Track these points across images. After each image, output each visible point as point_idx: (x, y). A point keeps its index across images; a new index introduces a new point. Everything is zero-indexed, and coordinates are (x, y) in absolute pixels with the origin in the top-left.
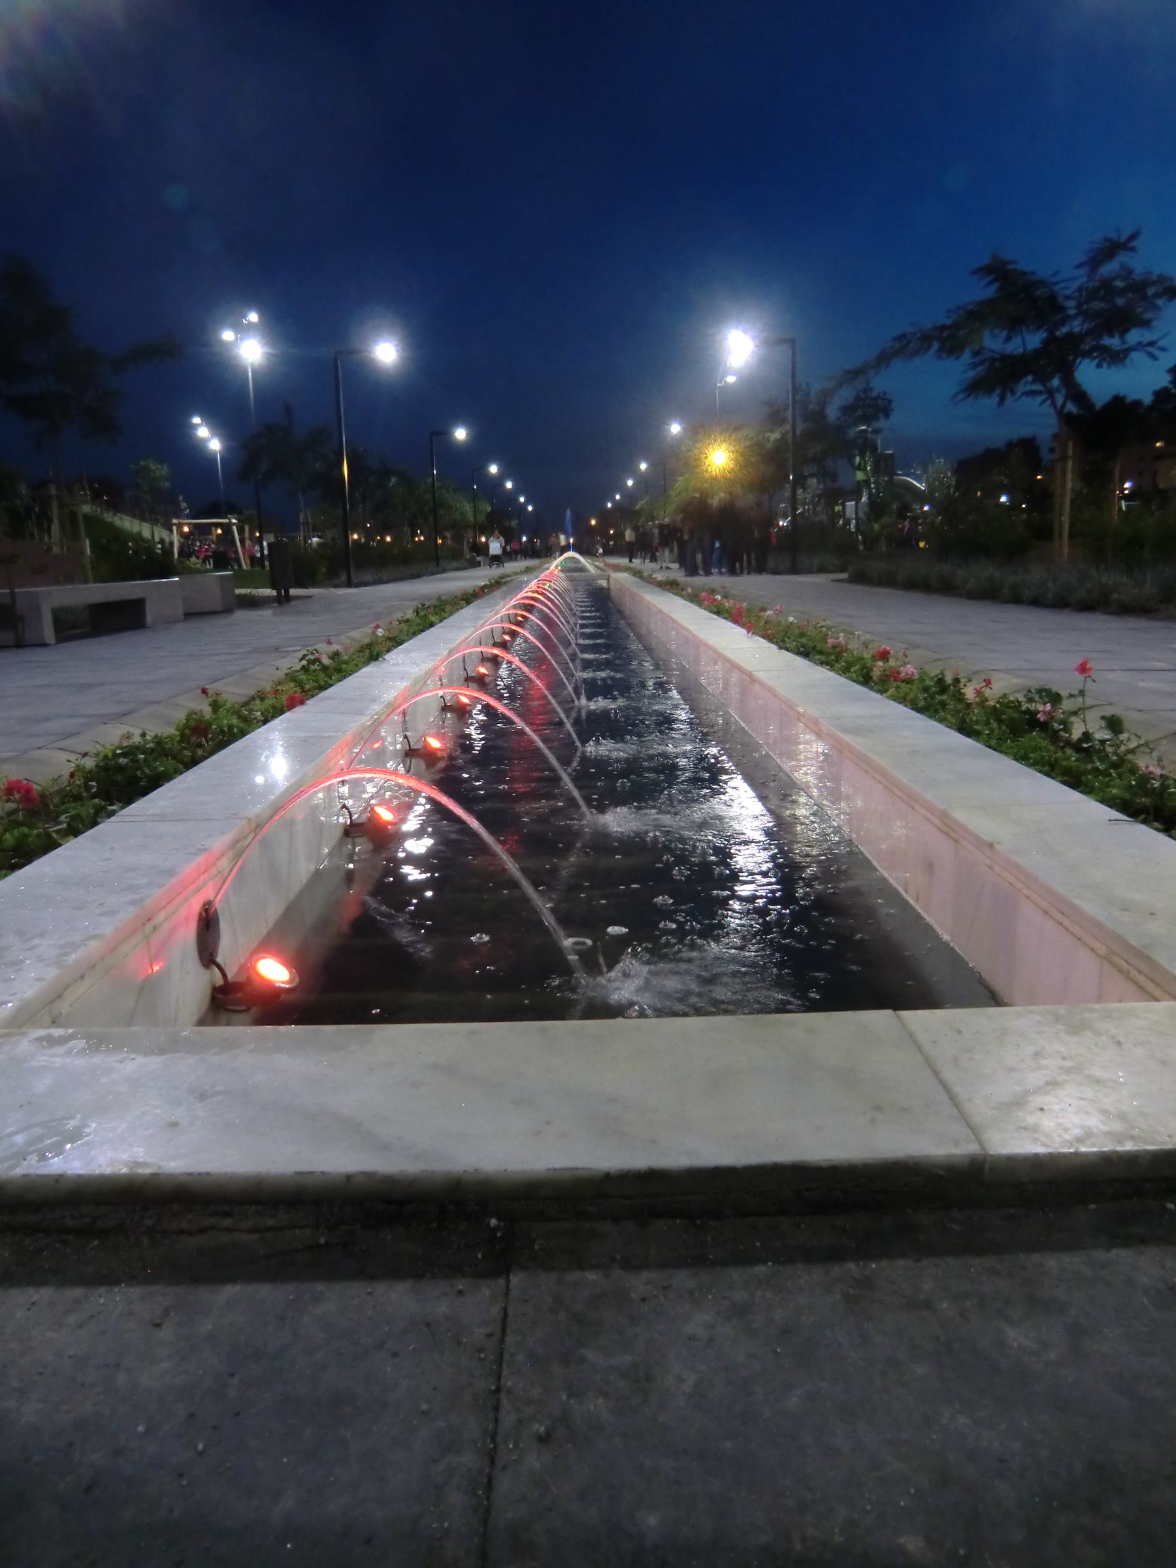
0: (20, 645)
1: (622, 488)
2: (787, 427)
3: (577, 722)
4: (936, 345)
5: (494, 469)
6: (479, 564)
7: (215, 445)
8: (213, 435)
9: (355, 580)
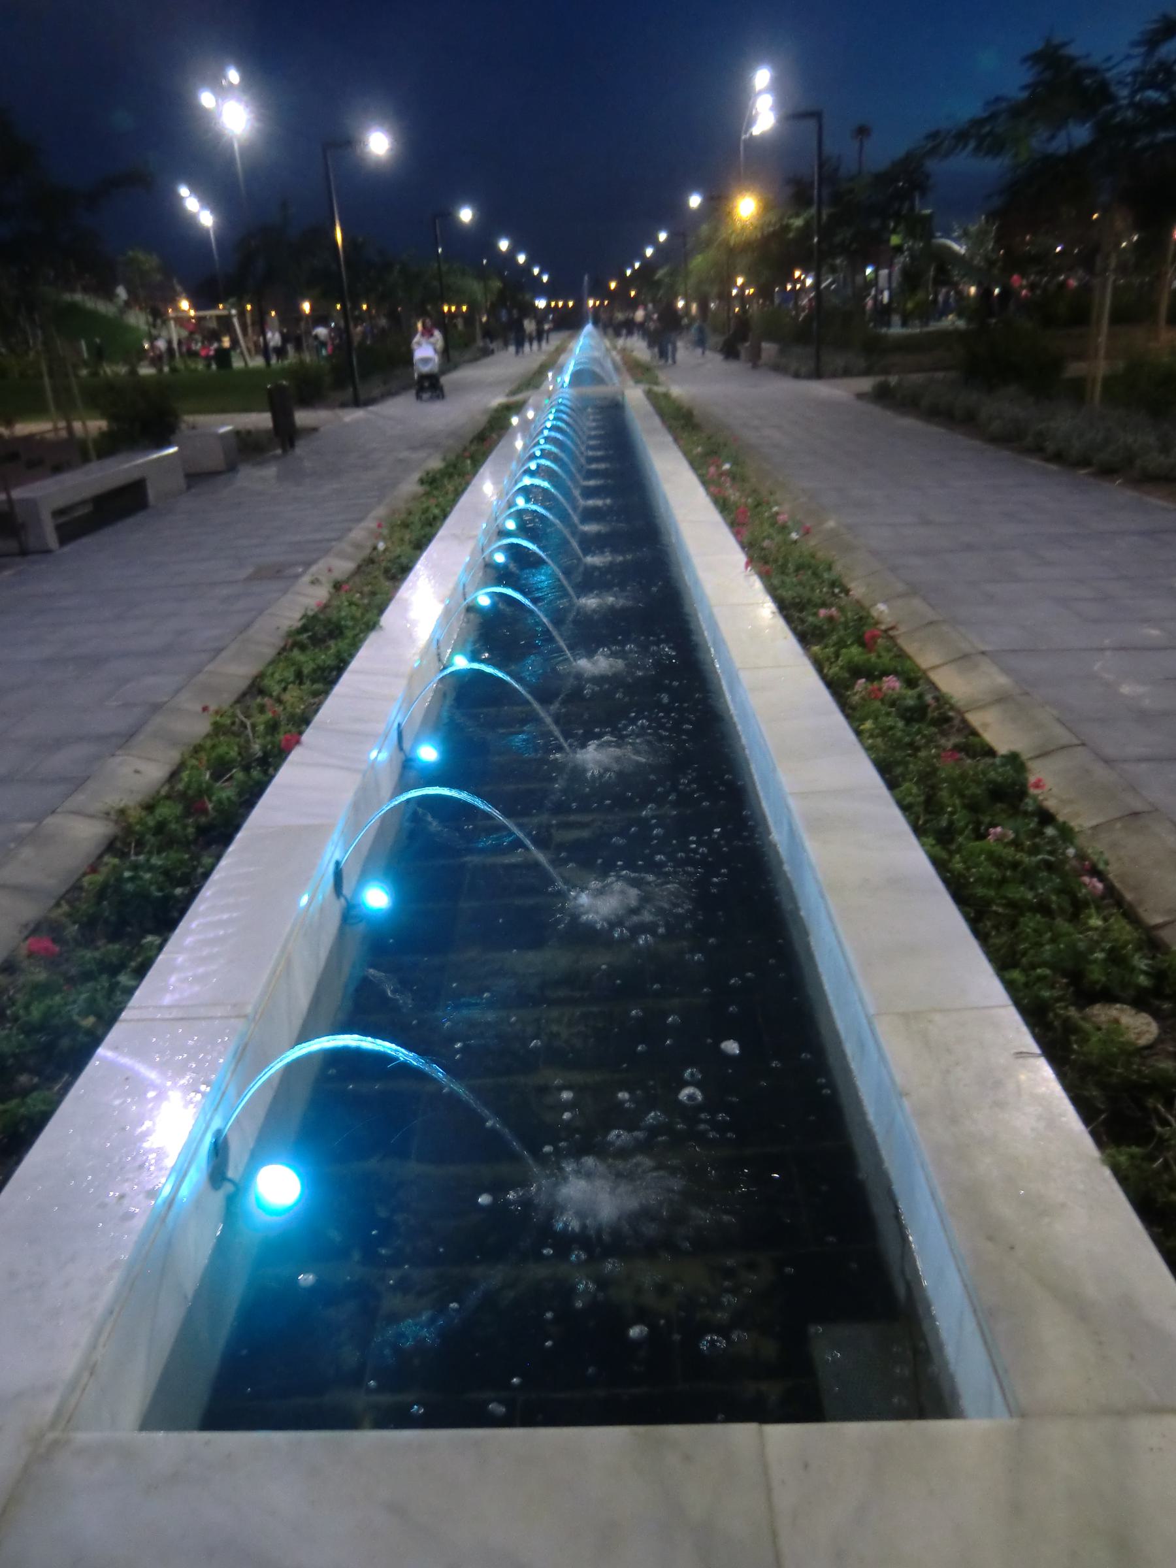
0: (24, 552)
1: (642, 256)
2: (813, 210)
3: (581, 543)
4: (972, 144)
5: (504, 245)
6: (492, 352)
7: (207, 219)
8: (203, 207)
9: (363, 396)
